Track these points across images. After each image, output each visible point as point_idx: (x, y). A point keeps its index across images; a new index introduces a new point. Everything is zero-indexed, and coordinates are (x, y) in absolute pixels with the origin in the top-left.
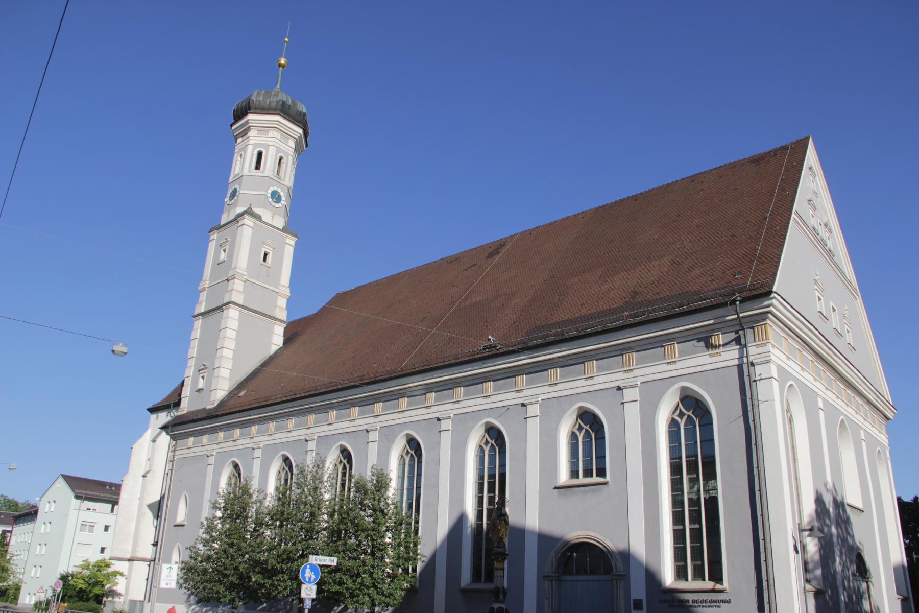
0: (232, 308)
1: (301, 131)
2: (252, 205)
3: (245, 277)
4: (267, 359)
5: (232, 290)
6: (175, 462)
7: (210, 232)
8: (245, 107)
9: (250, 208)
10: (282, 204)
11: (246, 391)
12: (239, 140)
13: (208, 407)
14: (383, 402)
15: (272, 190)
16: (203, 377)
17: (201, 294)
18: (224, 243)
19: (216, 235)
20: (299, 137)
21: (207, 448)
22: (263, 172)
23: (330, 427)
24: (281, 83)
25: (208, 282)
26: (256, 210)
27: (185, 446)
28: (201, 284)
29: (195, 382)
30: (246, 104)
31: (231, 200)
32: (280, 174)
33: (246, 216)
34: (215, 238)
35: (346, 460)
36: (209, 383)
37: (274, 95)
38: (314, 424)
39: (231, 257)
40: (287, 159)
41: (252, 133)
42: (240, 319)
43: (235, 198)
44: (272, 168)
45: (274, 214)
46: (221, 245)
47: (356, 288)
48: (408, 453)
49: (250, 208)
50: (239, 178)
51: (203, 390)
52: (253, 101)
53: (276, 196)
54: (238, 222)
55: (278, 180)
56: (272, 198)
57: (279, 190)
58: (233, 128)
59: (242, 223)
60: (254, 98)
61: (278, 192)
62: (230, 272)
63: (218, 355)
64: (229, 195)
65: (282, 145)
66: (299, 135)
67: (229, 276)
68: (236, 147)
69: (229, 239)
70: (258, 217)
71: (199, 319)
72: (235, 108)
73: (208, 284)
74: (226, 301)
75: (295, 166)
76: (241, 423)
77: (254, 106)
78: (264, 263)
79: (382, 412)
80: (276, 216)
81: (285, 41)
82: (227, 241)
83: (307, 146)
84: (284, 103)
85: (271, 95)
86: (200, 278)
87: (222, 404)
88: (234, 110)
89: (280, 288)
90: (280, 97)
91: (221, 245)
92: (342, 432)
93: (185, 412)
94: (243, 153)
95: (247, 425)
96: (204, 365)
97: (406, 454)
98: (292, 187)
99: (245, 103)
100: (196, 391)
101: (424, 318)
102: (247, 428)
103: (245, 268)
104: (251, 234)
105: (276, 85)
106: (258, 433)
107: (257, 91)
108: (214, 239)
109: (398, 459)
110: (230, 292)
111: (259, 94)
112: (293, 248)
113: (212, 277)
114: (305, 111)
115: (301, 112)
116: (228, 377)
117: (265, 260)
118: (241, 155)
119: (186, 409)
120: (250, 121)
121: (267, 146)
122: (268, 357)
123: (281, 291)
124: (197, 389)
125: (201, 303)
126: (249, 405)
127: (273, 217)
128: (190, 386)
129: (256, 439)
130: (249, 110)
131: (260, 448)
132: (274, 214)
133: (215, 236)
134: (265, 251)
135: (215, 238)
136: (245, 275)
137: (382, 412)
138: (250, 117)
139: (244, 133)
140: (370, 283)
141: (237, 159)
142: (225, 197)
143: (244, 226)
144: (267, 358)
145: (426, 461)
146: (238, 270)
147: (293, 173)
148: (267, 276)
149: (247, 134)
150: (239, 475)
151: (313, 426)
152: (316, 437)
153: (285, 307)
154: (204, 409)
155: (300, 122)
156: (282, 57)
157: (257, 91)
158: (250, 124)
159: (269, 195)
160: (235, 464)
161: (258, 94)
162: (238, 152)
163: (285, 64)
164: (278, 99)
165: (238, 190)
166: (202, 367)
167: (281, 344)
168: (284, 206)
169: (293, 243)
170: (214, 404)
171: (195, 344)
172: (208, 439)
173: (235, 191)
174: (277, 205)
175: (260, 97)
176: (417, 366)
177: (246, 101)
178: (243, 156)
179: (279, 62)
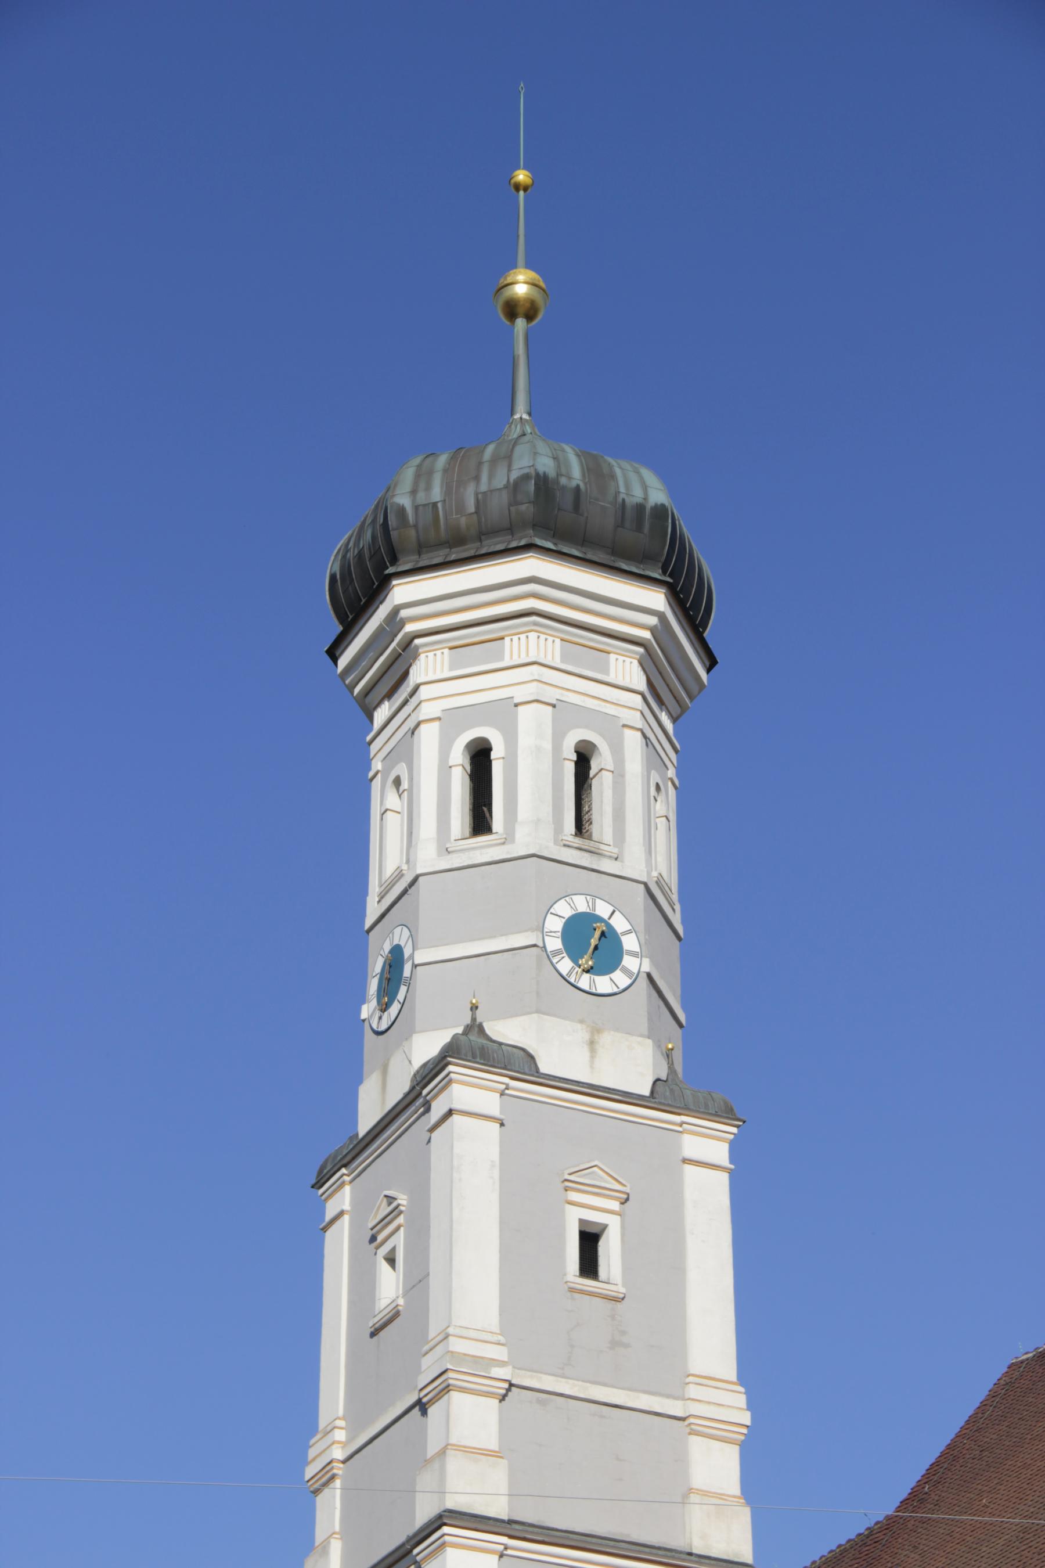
0: (734, 1497)
3: (498, 1372)
10: (627, 971)
22: (508, 839)
25: (340, 1435)
28: (312, 1453)
45: (596, 1031)
55: (585, 860)
57: (603, 910)
66: (653, 621)
80: (607, 1039)
81: (517, 187)
120: (404, 613)
127: (592, 1043)
136: (502, 1364)
148: (615, 1344)
158: (410, 628)
159: (554, 943)
165: (407, 952)
174: (603, 984)
175: (428, 488)
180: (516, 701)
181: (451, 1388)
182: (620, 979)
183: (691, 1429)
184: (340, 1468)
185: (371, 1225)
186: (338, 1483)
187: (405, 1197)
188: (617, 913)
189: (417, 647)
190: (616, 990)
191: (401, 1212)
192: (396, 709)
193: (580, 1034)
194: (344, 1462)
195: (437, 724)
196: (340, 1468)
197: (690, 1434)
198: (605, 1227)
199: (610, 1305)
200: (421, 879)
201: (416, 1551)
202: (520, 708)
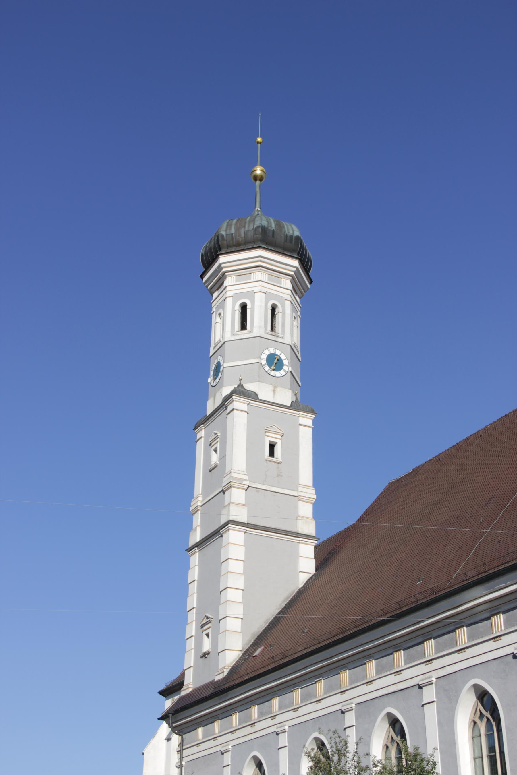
0: (301, 501)
1: (295, 263)
2: (242, 381)
3: (245, 483)
4: (295, 595)
5: (229, 504)
6: (183, 768)
7: (195, 429)
8: (215, 248)
9: (241, 386)
10: (284, 370)
11: (263, 647)
12: (215, 295)
13: (217, 678)
14: (435, 638)
15: (268, 353)
16: (207, 635)
17: (194, 516)
18: (214, 440)
19: (203, 430)
20: (294, 272)
21: (220, 740)
23: (371, 687)
24: (260, 202)
25: (200, 499)
26: (249, 387)
27: (192, 743)
28: (192, 504)
29: (199, 644)
30: (214, 243)
31: (215, 379)
32: (276, 329)
33: (234, 397)
34: (203, 435)
35: (399, 736)
36: (214, 644)
37: (250, 222)
38: (349, 685)
39: (223, 458)
40: (283, 306)
41: (229, 281)
42: (246, 544)
43: (220, 376)
44: (263, 323)
45: (275, 387)
46: (210, 445)
47: (414, 470)
48: (481, 716)
49: (241, 386)
50: (221, 346)
51: (208, 654)
52: (222, 236)
53: (275, 362)
54: (227, 408)
55: (273, 338)
56: (270, 366)
57: (278, 353)
58: (205, 279)
59: (231, 409)
60: (223, 233)
61: (277, 355)
62: (225, 479)
63: (222, 601)
64: (212, 373)
65: (272, 289)
66: (295, 269)
67: (224, 484)
68: (213, 304)
69: (219, 434)
70: (253, 396)
71: (196, 552)
72: (203, 252)
73: (201, 501)
74: (223, 521)
75: (299, 313)
76: (257, 696)
77: (225, 242)
78: (271, 458)
79: (436, 653)
80: (278, 390)
81: (258, 143)
82: (217, 437)
83: (311, 282)
84: (264, 230)
85: (245, 223)
86: (191, 495)
87: (234, 670)
88: (202, 255)
89: (300, 489)
90: (258, 223)
91: (210, 445)
92: (395, 690)
93: (190, 690)
94: (221, 311)
95: (267, 698)
96: (208, 618)
97: (391, 743)
98: (298, 345)
99: (213, 243)
100: (201, 657)
101: (490, 499)
102: (266, 703)
103: (245, 471)
104: (245, 421)
105: (255, 208)
106: (280, 708)
107: (227, 221)
108: (201, 437)
109: (469, 728)
110: (227, 508)
111: (229, 226)
112: (311, 429)
113: (205, 493)
114: (297, 233)
115: (291, 236)
116: (239, 630)
117: (272, 453)
118: (220, 314)
119: (191, 686)
120: (223, 265)
121: (251, 295)
122: (296, 591)
123: (300, 494)
124: (201, 654)
125: (195, 530)
126: (264, 667)
127: (274, 391)
128: (193, 651)
129: (279, 719)
130: (220, 250)
131: (285, 732)
132: (275, 387)
133: (202, 433)
134: (270, 441)
135: (203, 435)
136: (247, 480)
137: (436, 653)
138: (222, 259)
139: (219, 284)
140: (431, 460)
141: (216, 320)
142: (209, 377)
143: (234, 411)
144: (294, 594)
145: (507, 728)
146: (233, 475)
147: (297, 323)
148: (278, 476)
149: (223, 283)
150: (403, 736)
151: (349, 688)
152: (354, 705)
153: (311, 515)
154: (213, 683)
155: (293, 251)
156: (257, 165)
157: (227, 221)
158: (224, 270)
159: (264, 362)
160: (258, 762)
161: (227, 225)
162: (217, 311)
163: (263, 174)
164: (255, 226)
165: (222, 363)
166: (205, 621)
167: (313, 571)
168: (289, 374)
169: (310, 423)
170: (223, 672)
171: (193, 588)
172: (221, 726)
173: (218, 366)
174: (278, 374)
175: (230, 229)
176: (470, 574)
177: (214, 239)
178: (222, 315)
179: (254, 173)
180: (255, 292)
181: (232, 487)
182: (283, 372)
183: (299, 499)
184: (200, 508)
185: (210, 441)
186: (199, 512)
187: (220, 433)
188: (282, 353)
189: (226, 275)
190: (281, 376)
191: (218, 437)
192: (247, 693)
193: (271, 388)
194: (201, 506)
195: (231, 298)
196: (200, 508)
197: (299, 501)
198: (276, 443)
199: (277, 465)
200: (226, 342)
201: (221, 531)
202: (256, 294)
